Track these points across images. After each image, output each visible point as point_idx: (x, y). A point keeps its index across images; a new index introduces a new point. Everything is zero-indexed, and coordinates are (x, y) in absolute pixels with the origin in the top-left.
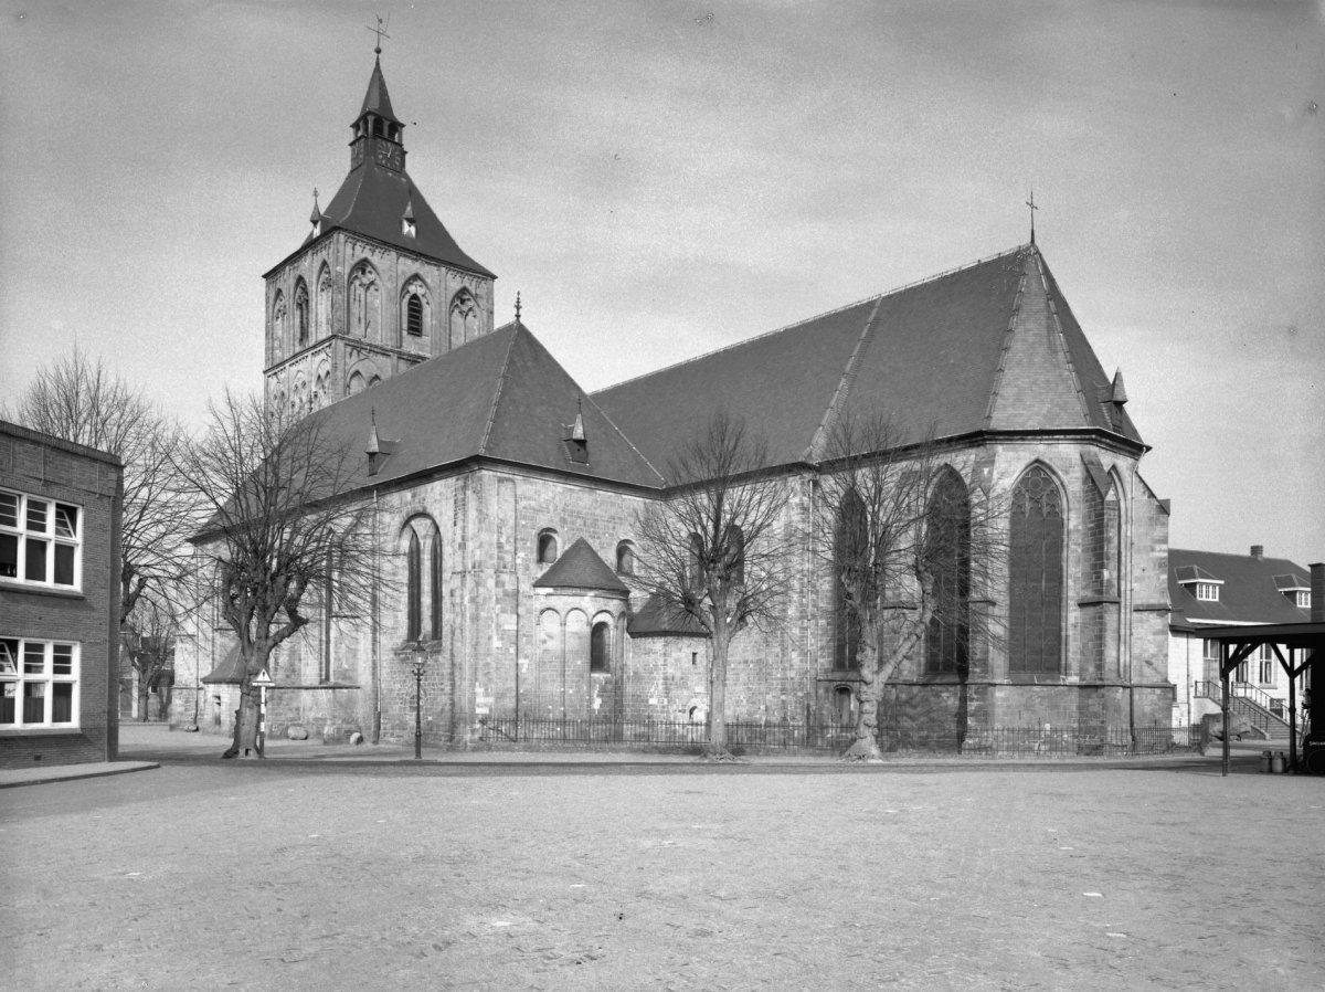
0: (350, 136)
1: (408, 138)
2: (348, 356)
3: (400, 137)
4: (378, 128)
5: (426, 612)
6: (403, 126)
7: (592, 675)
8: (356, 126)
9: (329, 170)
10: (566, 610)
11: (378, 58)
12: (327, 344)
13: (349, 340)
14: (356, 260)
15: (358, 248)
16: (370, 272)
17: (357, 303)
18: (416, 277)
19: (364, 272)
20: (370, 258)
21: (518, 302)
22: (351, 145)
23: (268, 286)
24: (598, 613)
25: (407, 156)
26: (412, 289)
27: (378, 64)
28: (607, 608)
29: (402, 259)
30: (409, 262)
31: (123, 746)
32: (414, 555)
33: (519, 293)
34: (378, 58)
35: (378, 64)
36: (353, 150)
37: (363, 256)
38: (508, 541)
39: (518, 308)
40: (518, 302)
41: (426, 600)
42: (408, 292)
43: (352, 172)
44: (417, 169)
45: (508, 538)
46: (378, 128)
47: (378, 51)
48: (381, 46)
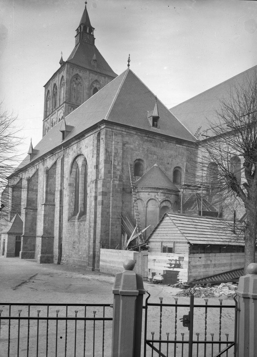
0: (76, 33)
1: (96, 34)
2: (70, 110)
3: (93, 33)
4: (85, 32)
5: (80, 202)
6: (94, 29)
7: (244, 245)
8: (77, 30)
9: (67, 47)
10: (147, 201)
11: (86, 6)
12: (62, 106)
13: (70, 104)
14: (74, 74)
15: (75, 70)
16: (79, 79)
17: (74, 90)
18: (96, 81)
19: (77, 79)
20: (79, 73)
21: (129, 59)
22: (75, 37)
23: (45, 89)
24: (163, 202)
25: (95, 40)
26: (95, 85)
27: (86, 7)
28: (169, 199)
29: (91, 75)
30: (94, 75)
31: (101, 265)
32: (76, 172)
33: (129, 55)
34: (86, 6)
35: (86, 7)
36: (76, 39)
37: (76, 73)
38: (118, 165)
39: (129, 61)
40: (129, 59)
41: (81, 196)
42: (93, 86)
43: (75, 47)
44: (98, 44)
45: (118, 163)
46: (85, 32)
47: (86, 3)
48: (87, 2)
